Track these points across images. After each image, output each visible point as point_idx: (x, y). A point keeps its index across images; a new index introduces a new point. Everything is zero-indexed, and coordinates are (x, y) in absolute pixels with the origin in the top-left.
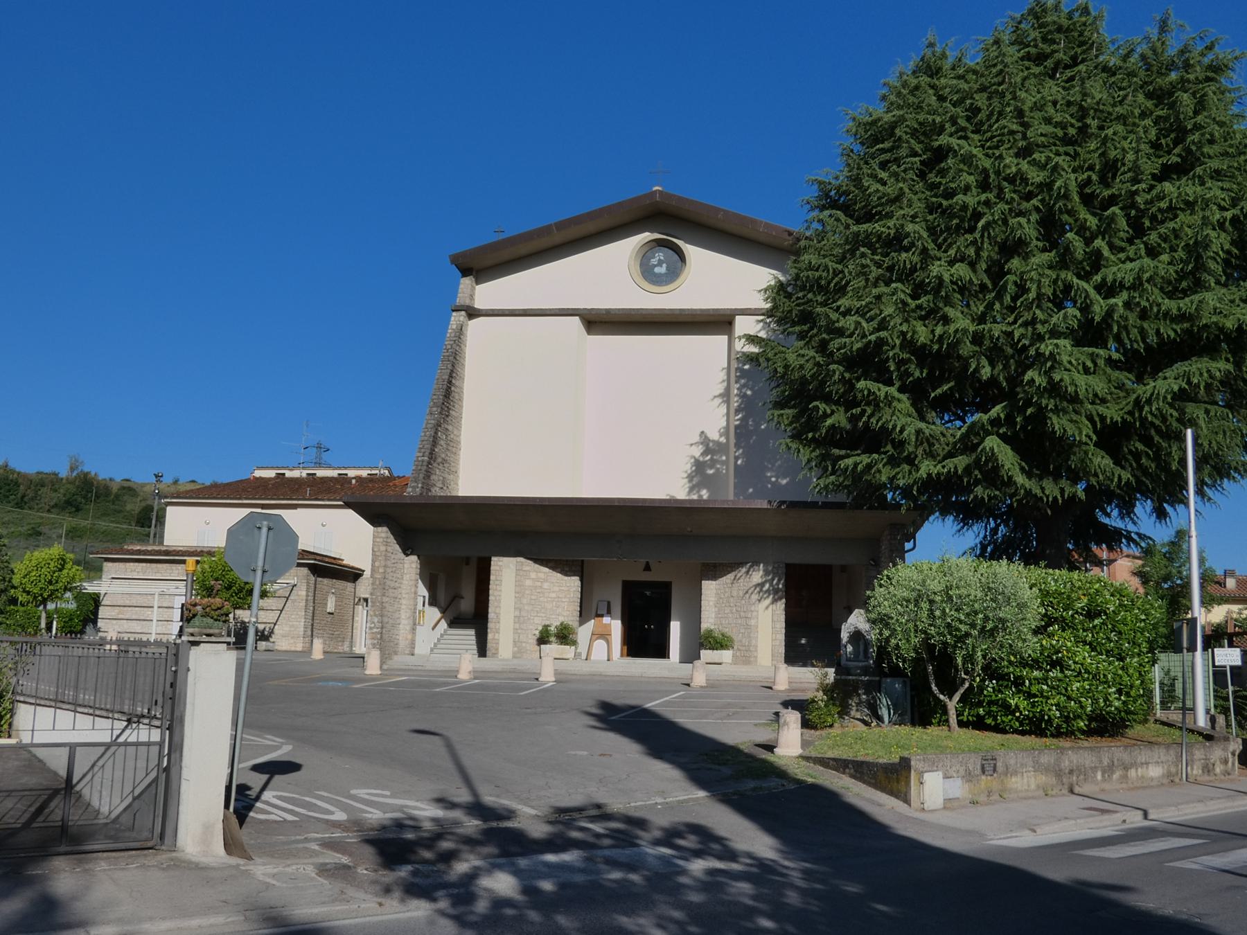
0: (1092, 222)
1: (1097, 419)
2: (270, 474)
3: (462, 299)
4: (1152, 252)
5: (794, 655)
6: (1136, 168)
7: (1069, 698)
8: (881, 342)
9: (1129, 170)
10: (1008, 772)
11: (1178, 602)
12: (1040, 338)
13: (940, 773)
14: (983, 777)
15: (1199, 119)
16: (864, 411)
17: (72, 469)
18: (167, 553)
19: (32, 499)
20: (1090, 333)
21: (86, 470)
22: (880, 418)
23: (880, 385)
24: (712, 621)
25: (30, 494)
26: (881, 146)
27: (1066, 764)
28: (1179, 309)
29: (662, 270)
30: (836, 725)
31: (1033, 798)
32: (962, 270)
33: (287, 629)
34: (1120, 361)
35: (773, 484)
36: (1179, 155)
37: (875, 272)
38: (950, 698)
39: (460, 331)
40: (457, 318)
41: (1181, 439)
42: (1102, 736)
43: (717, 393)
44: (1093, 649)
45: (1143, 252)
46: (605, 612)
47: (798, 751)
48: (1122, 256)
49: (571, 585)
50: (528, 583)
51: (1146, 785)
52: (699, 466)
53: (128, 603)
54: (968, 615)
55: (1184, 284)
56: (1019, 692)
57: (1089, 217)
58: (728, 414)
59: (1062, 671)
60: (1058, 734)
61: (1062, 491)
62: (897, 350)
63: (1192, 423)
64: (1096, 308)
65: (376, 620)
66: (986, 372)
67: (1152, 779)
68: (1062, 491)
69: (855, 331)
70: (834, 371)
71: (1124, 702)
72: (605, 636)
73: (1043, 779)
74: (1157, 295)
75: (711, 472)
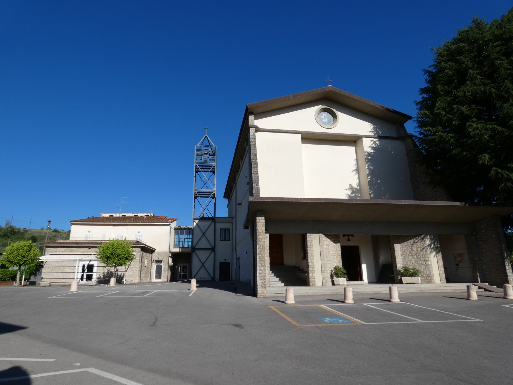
5: (449, 280)
17: (7, 225)
18: (72, 243)
33: (131, 273)
38: (87, 272)
43: (354, 169)
53: (57, 265)
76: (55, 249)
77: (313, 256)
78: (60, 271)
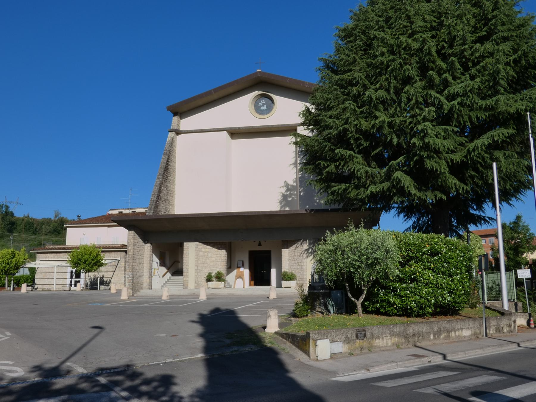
0: (444, 65)
1: (449, 161)
2: (116, 212)
3: (174, 126)
4: (472, 78)
6: (464, 38)
7: (421, 297)
8: (345, 130)
9: (461, 39)
10: (373, 337)
11: (518, 250)
12: (419, 123)
13: (328, 340)
14: (358, 341)
15: (495, 13)
16: (340, 164)
17: (56, 216)
19: (40, 230)
20: (443, 119)
21: (62, 216)
22: (348, 166)
23: (347, 151)
24: (287, 267)
25: (39, 227)
26: (349, 39)
27: (410, 331)
28: (487, 105)
29: (264, 108)
30: (309, 315)
31: (389, 350)
32: (381, 93)
34: (458, 131)
35: (318, 203)
36: (486, 31)
37: (342, 98)
39: (173, 140)
40: (171, 135)
41: (492, 168)
42: (445, 316)
43: (292, 163)
44: (434, 271)
45: (468, 78)
46: (241, 265)
47: (276, 329)
48: (459, 81)
49: (222, 254)
50: (201, 253)
51: (461, 340)
52: (285, 197)
53: (47, 271)
54: (359, 257)
55: (490, 92)
56: (395, 295)
57: (442, 64)
58: (296, 172)
59: (417, 284)
60: (418, 316)
61: (436, 196)
62: (354, 133)
63: (497, 160)
64: (445, 107)
65: (130, 274)
66: (395, 141)
67: (465, 337)
68: (436, 196)
69: (336, 126)
70: (326, 146)
71: (453, 298)
72: (240, 276)
73: (395, 340)
74: (476, 99)
75: (290, 199)
76: (44, 255)
77: (188, 263)
78: (50, 277)
